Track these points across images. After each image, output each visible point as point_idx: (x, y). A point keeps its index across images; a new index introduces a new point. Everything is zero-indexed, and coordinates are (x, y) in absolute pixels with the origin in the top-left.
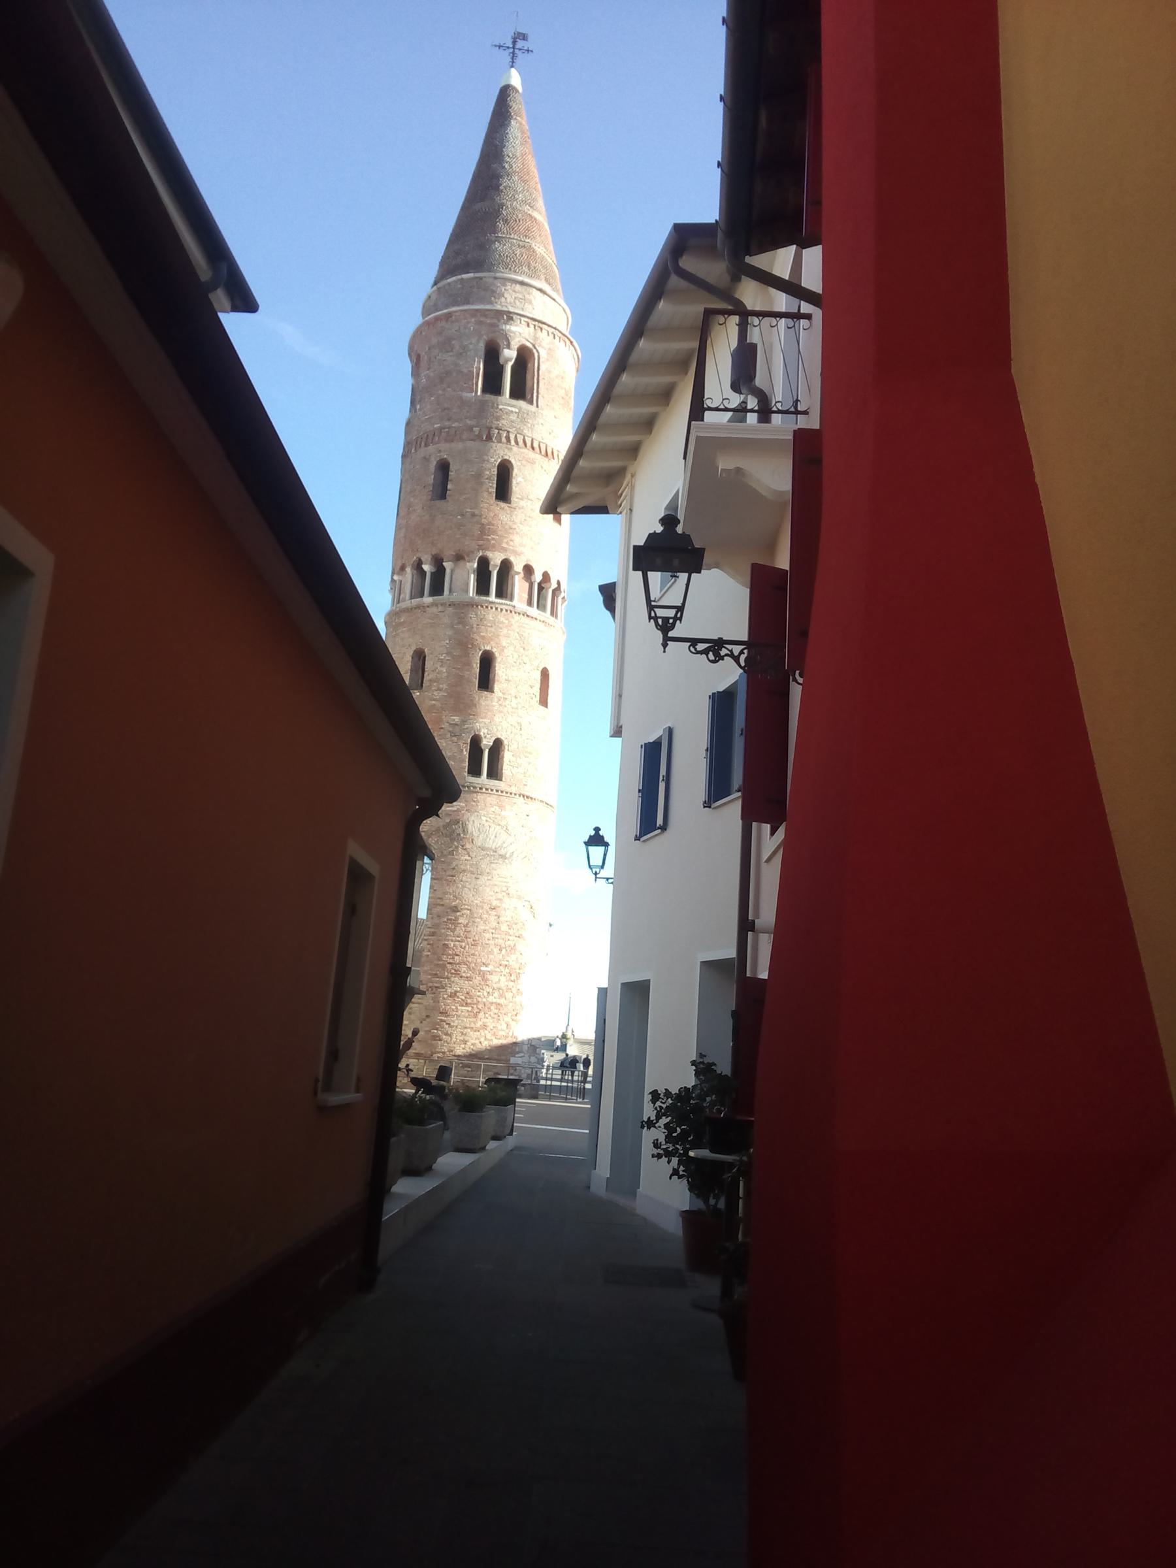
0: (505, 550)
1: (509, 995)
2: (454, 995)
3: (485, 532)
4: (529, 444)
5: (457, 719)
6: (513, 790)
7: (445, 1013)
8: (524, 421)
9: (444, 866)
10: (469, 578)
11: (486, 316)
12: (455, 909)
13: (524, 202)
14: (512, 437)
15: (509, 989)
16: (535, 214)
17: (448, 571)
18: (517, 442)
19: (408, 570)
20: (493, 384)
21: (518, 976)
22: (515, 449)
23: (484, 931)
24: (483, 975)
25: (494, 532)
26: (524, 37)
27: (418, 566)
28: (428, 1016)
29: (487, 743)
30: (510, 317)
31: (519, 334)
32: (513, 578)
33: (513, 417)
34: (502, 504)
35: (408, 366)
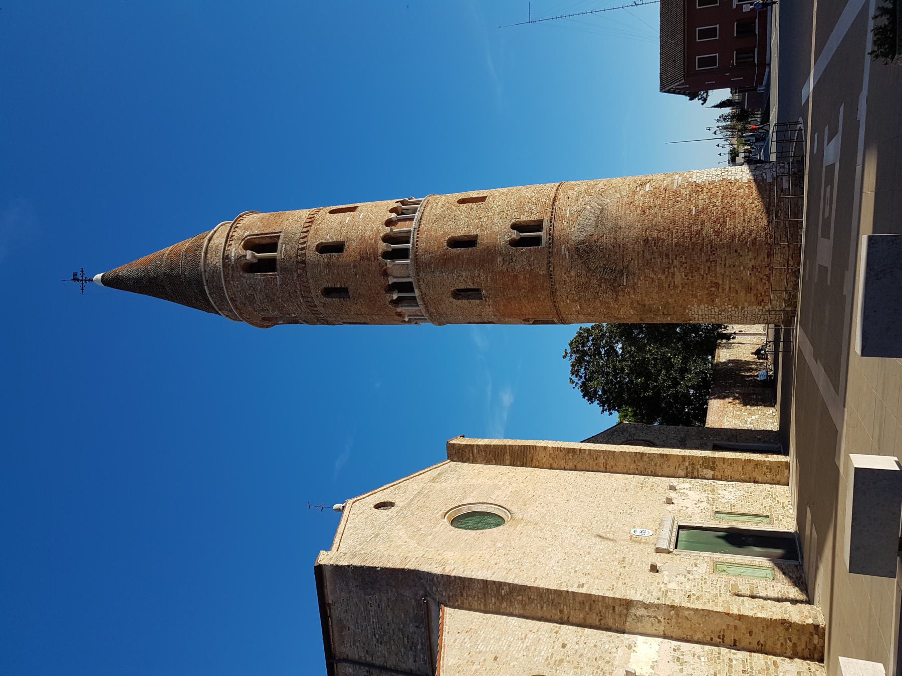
0: (376, 241)
1: (714, 191)
2: (717, 233)
3: (366, 256)
4: (305, 234)
5: (499, 259)
6: (549, 210)
7: (733, 238)
8: (290, 240)
9: (612, 254)
10: (398, 264)
11: (228, 274)
12: (646, 241)
13: (161, 260)
14: (301, 246)
15: (710, 191)
16: (168, 252)
17: (395, 280)
18: (305, 243)
19: (399, 310)
20: (269, 265)
21: (698, 185)
22: (309, 243)
23: (662, 216)
24: (698, 213)
25: (365, 250)
26: (75, 274)
27: (396, 302)
28: (736, 251)
29: (514, 234)
30: (226, 258)
31: (236, 250)
32: (396, 233)
33: (289, 247)
34: (346, 247)
35: (282, 329)
